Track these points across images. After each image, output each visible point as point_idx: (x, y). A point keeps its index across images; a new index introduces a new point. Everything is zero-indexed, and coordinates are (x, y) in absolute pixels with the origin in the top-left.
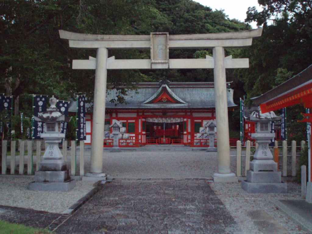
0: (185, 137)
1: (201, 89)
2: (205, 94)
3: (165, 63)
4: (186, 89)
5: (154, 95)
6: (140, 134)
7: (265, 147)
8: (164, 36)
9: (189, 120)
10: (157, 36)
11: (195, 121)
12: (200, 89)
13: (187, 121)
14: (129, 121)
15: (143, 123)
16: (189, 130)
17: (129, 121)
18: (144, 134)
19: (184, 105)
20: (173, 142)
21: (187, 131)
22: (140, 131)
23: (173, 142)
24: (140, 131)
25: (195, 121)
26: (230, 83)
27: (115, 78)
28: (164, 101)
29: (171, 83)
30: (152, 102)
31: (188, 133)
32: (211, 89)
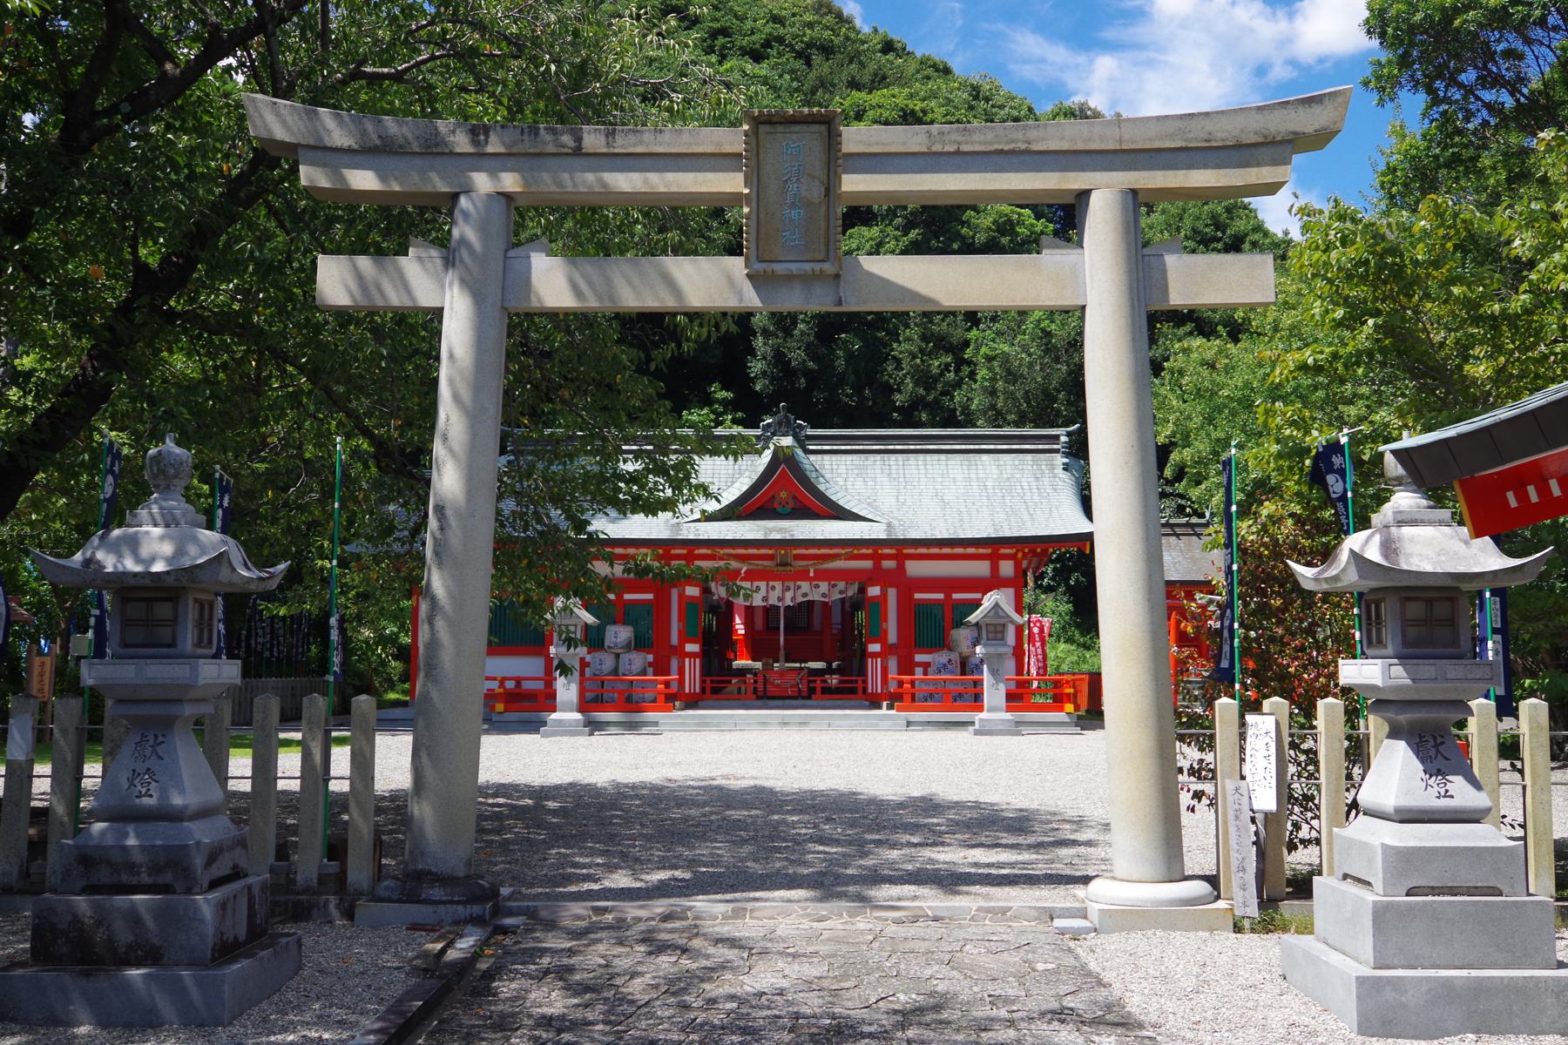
0: (874, 668)
1: (943, 456)
2: (960, 477)
3: (820, 277)
4: (878, 457)
5: (737, 485)
6: (675, 654)
7: (1436, 746)
8: (816, 128)
9: (892, 593)
10: (780, 128)
11: (918, 596)
12: (936, 456)
13: (884, 596)
14: (955, 596)
15: (681, 596)
16: (892, 637)
17: (955, 596)
18: (692, 655)
19: (876, 532)
20: (819, 690)
21: (881, 638)
22: (674, 640)
23: (819, 690)
24: (674, 640)
25: (918, 596)
26: (1069, 434)
27: (549, 371)
28: (780, 509)
29: (810, 432)
30: (731, 513)
31: (887, 650)
32: (985, 457)
